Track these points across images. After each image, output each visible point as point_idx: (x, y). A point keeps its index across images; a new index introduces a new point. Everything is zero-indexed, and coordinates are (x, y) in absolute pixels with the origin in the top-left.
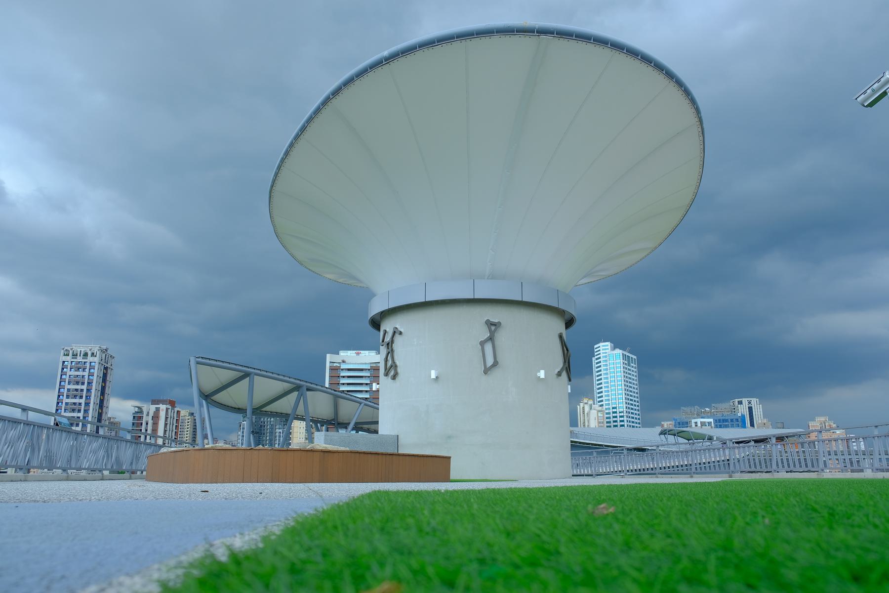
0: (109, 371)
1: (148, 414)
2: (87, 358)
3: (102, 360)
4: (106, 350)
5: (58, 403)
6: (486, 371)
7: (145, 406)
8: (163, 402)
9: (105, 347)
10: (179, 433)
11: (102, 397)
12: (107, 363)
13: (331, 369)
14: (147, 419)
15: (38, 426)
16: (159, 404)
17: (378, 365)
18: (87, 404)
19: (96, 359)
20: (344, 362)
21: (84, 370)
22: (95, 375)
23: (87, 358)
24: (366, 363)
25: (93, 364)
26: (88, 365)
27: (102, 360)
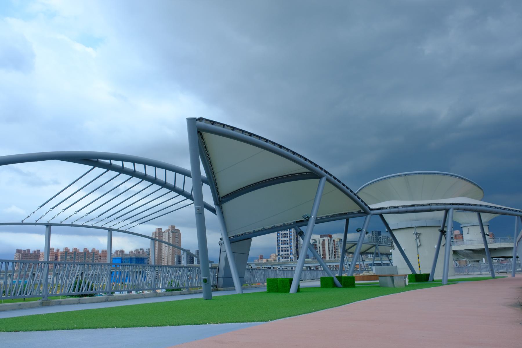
1: (319, 243)
5: (278, 241)
6: (418, 247)
8: (326, 236)
10: (336, 251)
11: (297, 236)
14: (319, 245)
16: (324, 237)
18: (291, 240)
22: (293, 246)
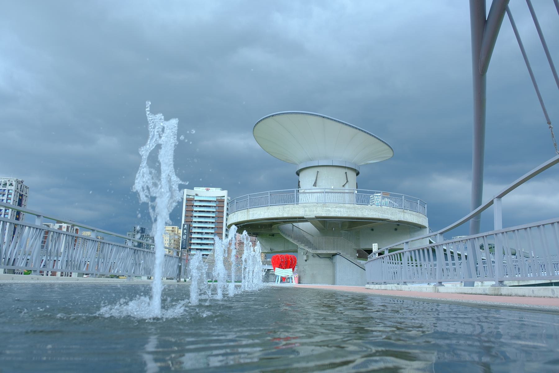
0: (24, 197)
2: (6, 187)
3: (17, 189)
4: (22, 182)
7: (51, 224)
9: (21, 180)
12: (23, 192)
13: (188, 200)
15: (130, 248)
17: (223, 198)
19: (13, 188)
20: (197, 195)
21: (3, 195)
22: (12, 199)
23: (6, 187)
24: (213, 197)
25: (10, 191)
26: (6, 192)
27: (17, 189)
